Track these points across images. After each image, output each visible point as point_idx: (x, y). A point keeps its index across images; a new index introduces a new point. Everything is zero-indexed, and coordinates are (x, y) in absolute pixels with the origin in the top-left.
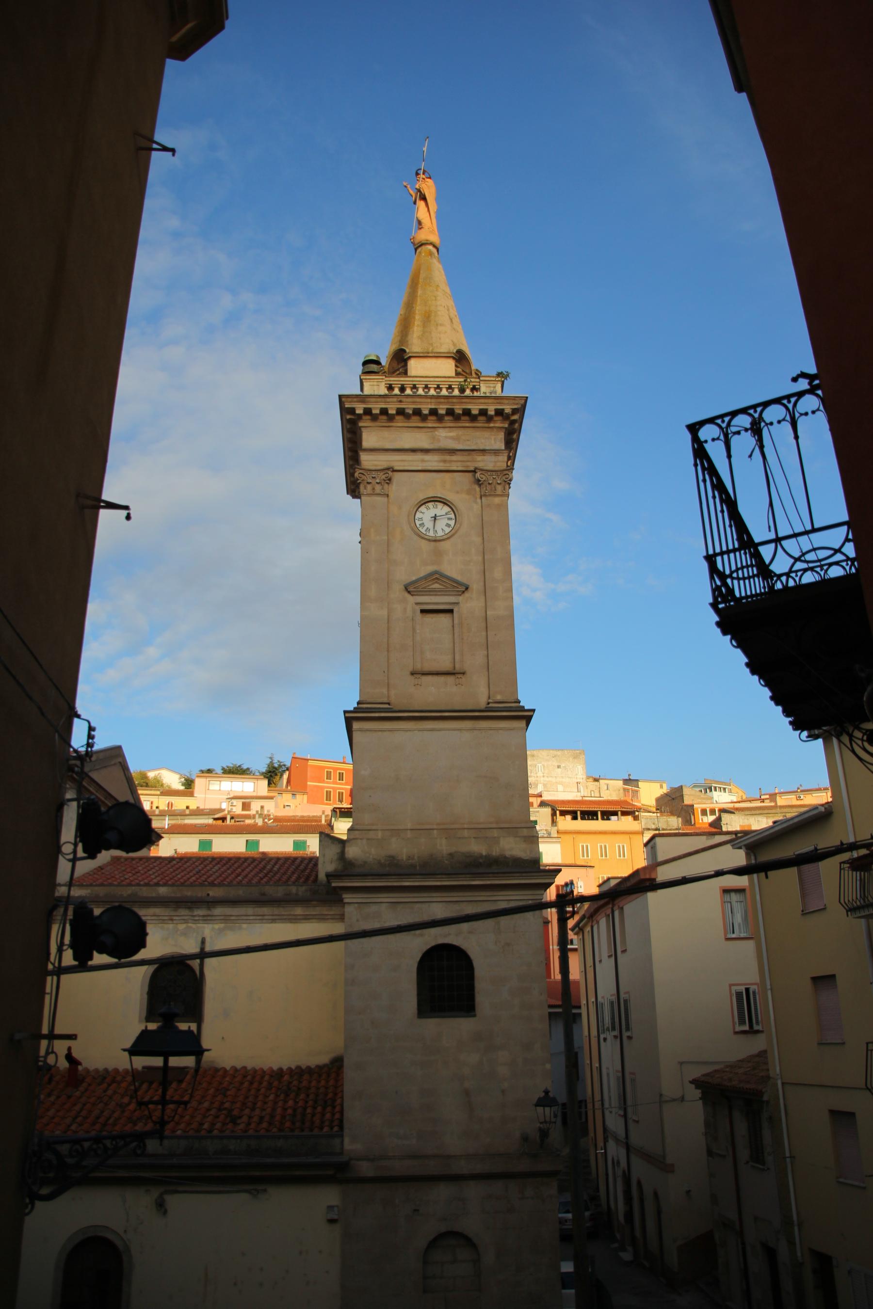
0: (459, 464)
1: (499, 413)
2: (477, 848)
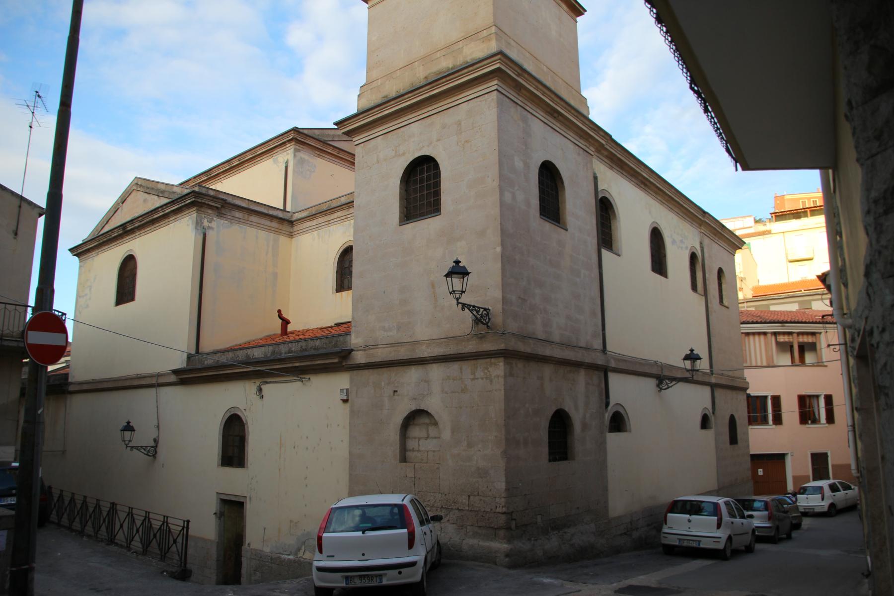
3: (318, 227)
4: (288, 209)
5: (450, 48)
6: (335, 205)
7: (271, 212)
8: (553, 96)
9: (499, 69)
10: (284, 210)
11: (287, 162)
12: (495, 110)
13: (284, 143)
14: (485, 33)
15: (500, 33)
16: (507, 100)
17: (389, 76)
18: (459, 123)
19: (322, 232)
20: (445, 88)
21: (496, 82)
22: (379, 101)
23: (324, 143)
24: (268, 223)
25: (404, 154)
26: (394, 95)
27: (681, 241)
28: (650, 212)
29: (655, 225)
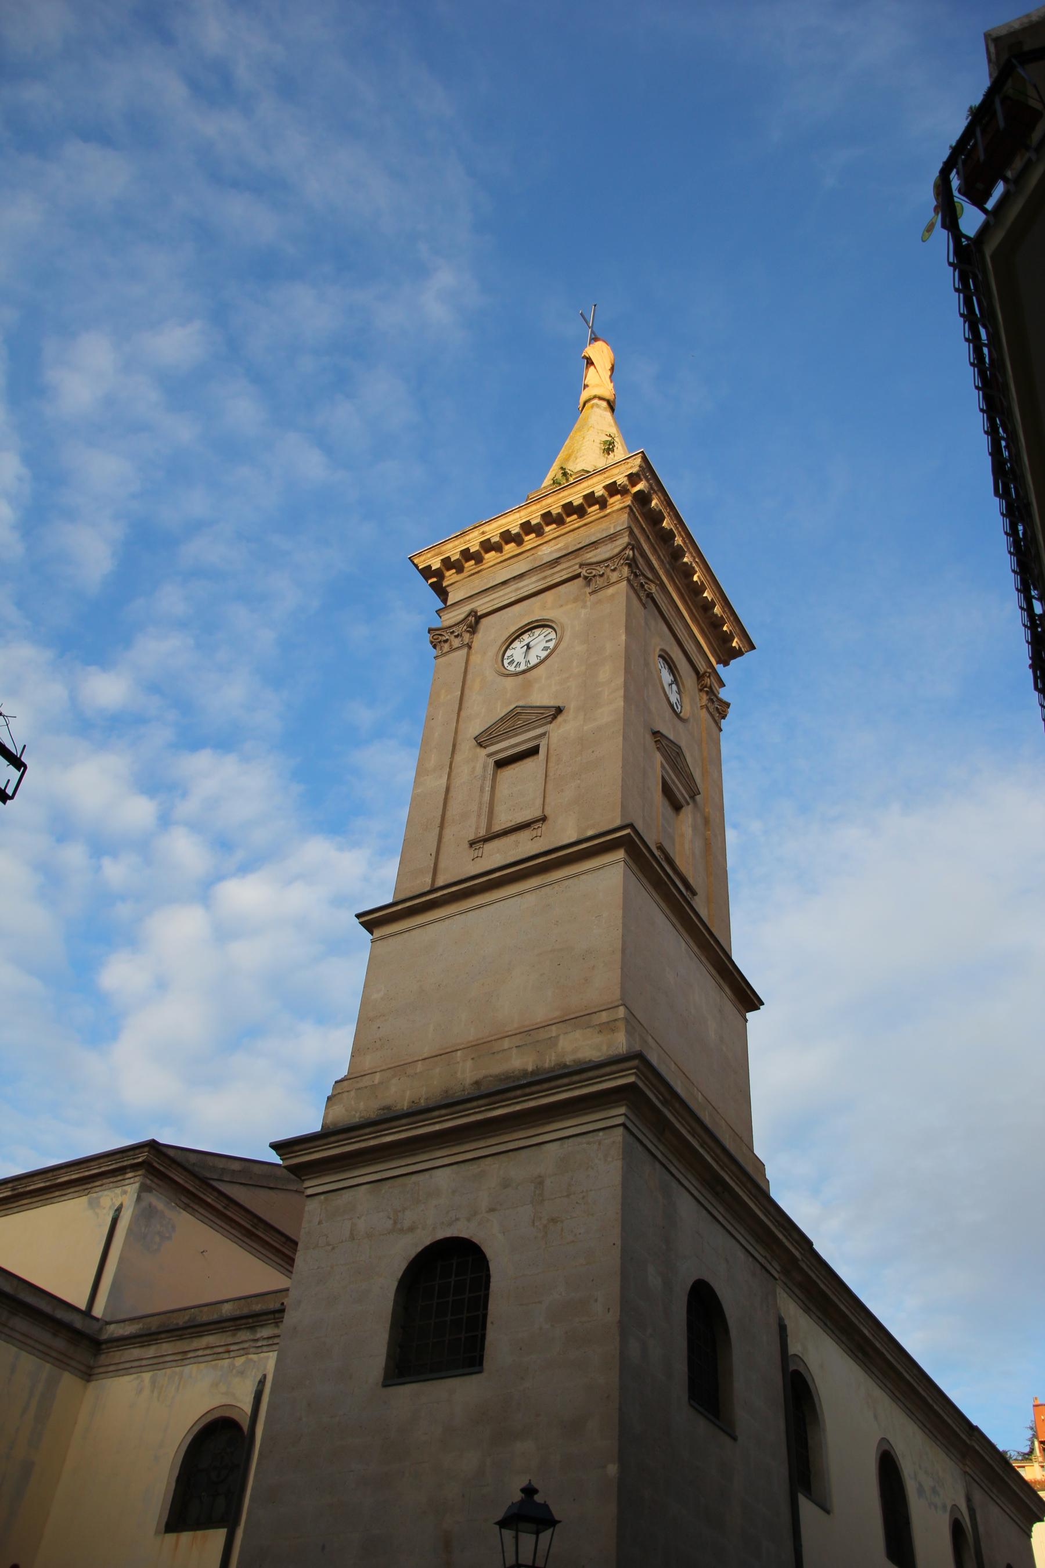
0: (564, 572)
1: (613, 489)
2: (521, 1062)
3: (157, 1364)
4: (98, 1311)
5: (529, 1035)
6: (205, 1318)
7: (60, 1314)
8: (719, 1151)
9: (632, 1086)
10: (87, 1313)
11: (119, 1210)
12: (619, 1164)
13: (122, 1170)
14: (604, 1017)
15: (632, 1022)
16: (640, 1148)
17: (400, 1069)
18: (539, 1182)
19: (163, 1376)
20: (518, 1108)
21: (623, 1110)
22: (373, 1115)
23: (205, 1182)
24: (46, 1337)
25: (412, 1229)
26: (404, 1105)
27: (934, 1490)
28: (876, 1417)
29: (887, 1447)
